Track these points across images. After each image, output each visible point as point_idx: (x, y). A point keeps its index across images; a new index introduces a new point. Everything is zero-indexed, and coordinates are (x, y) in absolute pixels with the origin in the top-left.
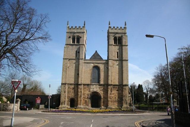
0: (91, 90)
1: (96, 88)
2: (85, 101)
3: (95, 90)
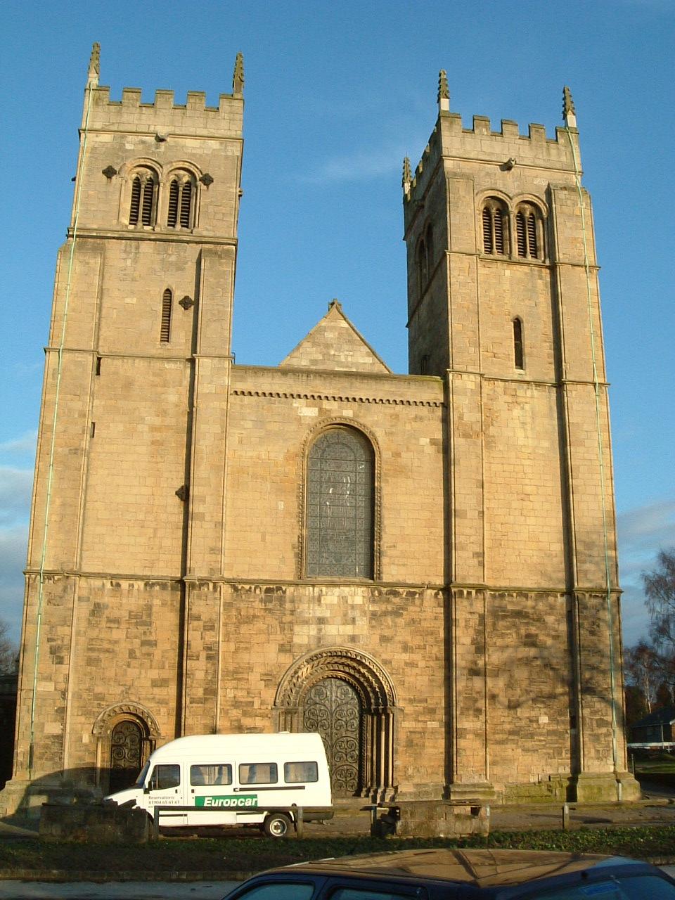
0: (304, 636)
3: (337, 634)
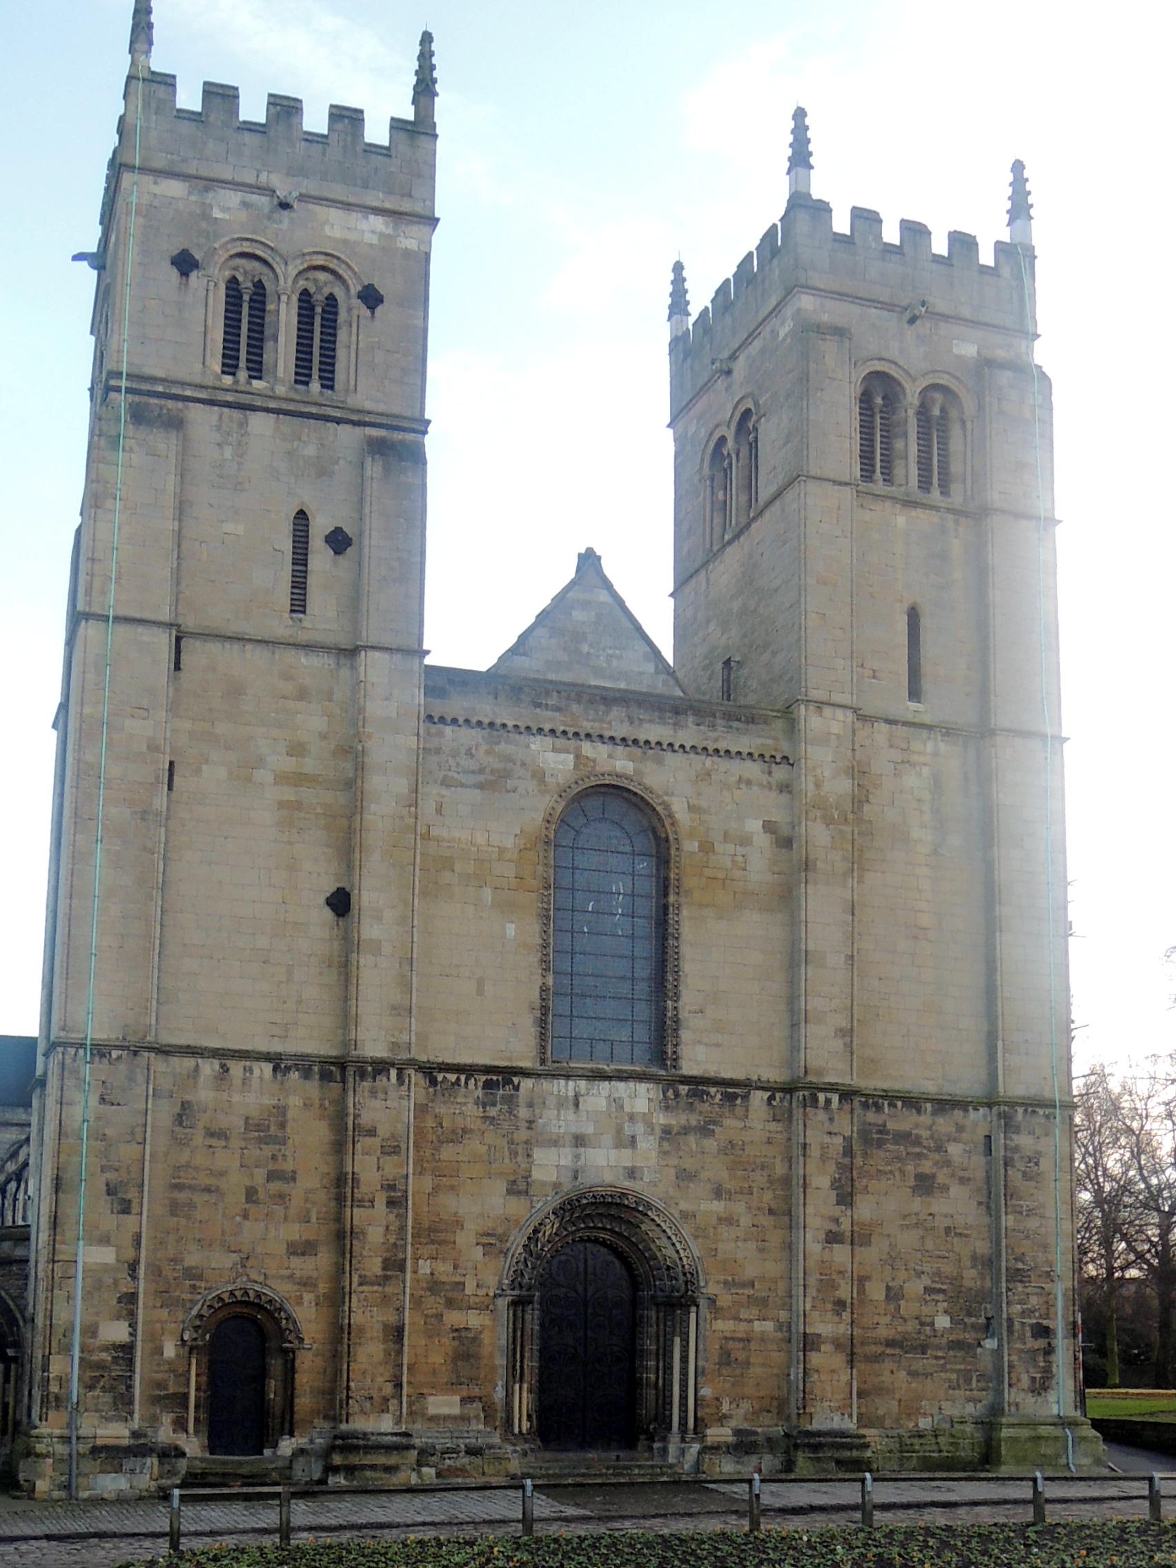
0: (550, 1167)
1: (601, 1134)
2: (447, 1342)
3: (604, 1166)
